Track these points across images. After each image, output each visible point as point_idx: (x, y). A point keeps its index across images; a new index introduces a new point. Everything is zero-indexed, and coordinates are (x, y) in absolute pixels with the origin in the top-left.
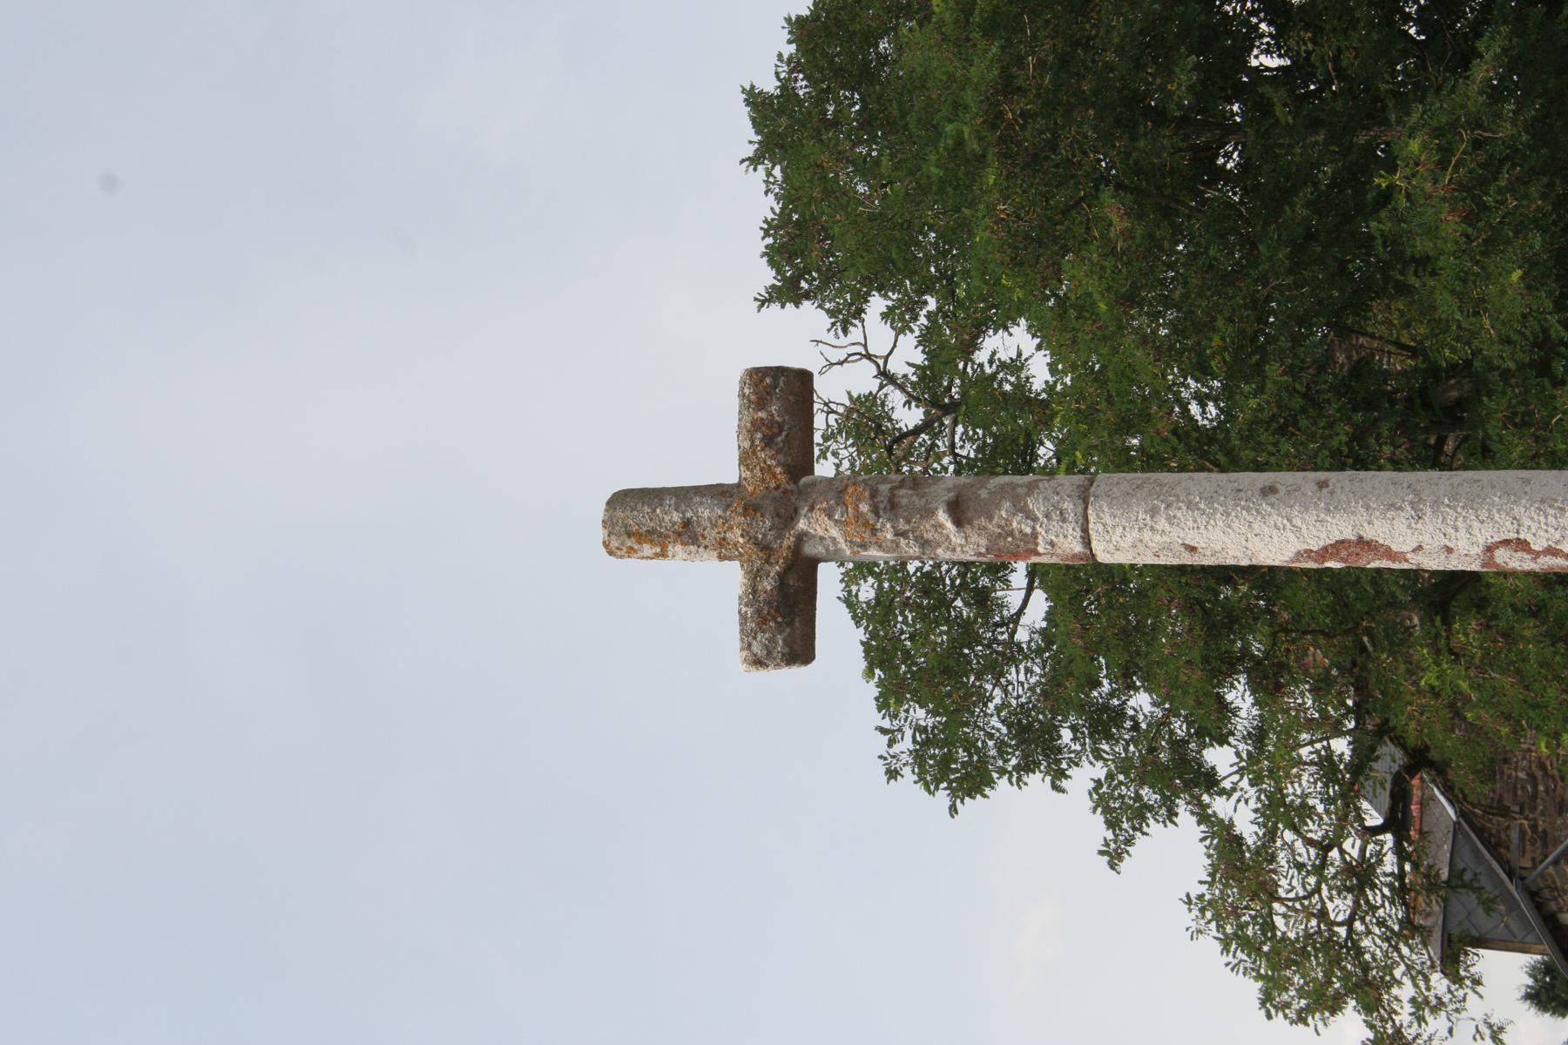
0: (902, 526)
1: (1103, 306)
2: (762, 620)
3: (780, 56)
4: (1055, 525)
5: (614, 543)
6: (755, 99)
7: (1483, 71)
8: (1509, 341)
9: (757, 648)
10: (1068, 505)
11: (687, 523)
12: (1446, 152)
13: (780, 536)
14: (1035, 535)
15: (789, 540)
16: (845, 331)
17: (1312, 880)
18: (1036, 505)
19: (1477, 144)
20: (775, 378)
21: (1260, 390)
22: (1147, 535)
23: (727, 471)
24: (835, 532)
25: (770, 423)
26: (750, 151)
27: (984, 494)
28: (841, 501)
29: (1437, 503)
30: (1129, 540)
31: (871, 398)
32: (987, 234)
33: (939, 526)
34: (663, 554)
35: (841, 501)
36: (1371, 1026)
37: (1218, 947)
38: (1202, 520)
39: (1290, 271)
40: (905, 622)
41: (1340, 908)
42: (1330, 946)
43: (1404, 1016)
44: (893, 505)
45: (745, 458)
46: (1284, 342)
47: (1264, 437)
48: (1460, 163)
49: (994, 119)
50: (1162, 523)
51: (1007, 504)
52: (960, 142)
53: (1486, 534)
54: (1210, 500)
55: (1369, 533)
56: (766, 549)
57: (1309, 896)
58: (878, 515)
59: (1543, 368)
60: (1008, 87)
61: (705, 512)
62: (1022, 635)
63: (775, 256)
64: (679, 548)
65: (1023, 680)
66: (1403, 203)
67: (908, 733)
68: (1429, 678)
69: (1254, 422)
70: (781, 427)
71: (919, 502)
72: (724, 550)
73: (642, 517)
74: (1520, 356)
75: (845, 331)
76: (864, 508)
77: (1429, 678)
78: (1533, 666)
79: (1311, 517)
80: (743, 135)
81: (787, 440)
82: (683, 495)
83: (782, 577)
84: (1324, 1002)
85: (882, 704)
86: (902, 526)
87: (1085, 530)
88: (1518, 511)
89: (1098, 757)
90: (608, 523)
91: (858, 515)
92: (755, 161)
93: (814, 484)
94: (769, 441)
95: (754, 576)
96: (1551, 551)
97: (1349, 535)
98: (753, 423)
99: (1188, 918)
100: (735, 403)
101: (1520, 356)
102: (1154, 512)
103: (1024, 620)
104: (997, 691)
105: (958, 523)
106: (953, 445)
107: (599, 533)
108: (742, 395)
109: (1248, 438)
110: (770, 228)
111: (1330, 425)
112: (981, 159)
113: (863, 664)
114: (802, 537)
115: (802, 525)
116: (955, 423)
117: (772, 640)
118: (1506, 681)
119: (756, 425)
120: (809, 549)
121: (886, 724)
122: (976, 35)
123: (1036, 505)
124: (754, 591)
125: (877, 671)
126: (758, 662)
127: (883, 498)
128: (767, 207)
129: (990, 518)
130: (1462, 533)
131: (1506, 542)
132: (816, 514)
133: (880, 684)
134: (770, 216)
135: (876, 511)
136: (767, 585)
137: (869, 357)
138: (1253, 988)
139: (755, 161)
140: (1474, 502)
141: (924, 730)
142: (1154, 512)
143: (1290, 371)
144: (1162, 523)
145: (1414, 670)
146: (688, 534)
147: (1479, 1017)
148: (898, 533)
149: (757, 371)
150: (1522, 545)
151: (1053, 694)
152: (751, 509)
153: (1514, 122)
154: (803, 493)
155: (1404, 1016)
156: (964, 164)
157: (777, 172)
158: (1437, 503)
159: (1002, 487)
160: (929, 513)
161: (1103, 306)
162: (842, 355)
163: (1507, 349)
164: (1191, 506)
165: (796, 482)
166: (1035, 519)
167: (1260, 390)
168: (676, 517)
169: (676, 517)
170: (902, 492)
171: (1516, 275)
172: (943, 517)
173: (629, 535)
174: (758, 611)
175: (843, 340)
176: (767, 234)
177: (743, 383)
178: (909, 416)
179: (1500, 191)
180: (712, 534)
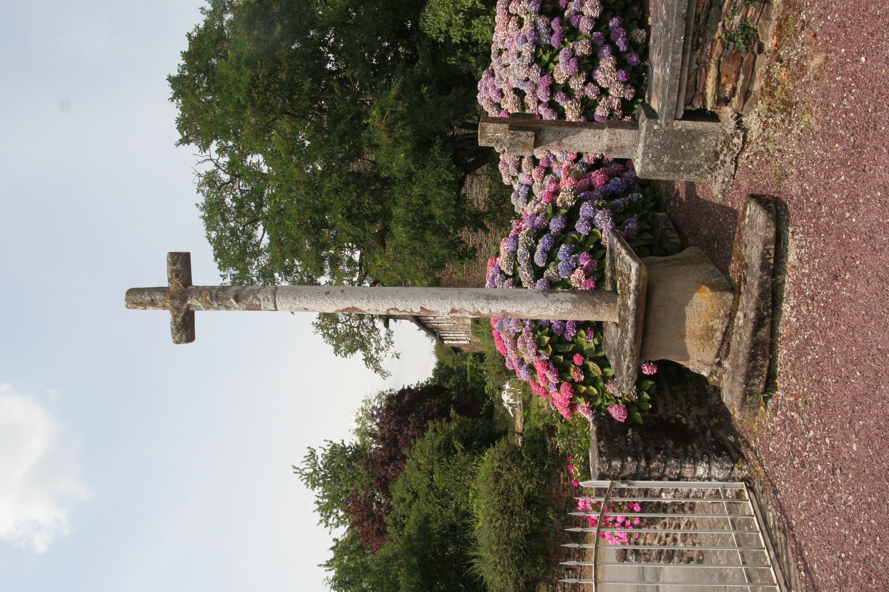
0: (220, 303)
1: (283, 155)
2: (178, 330)
3: (179, 65)
4: (266, 302)
5: (129, 306)
6: (171, 79)
7: (394, 92)
8: (400, 171)
9: (177, 338)
10: (269, 296)
11: (152, 300)
12: (383, 114)
13: (182, 305)
14: (260, 305)
15: (185, 307)
16: (205, 151)
17: (348, 317)
18: (260, 296)
19: (392, 112)
20: (178, 256)
21: (330, 181)
22: (293, 305)
23: (165, 283)
24: (199, 304)
25: (177, 271)
26: (171, 96)
27: (244, 293)
28: (200, 295)
29: (374, 298)
30: (288, 306)
31: (214, 172)
32: (247, 131)
33: (231, 303)
34: (145, 309)
35: (200, 295)
36: (365, 355)
37: (321, 336)
38: (309, 302)
39: (339, 145)
40: (226, 244)
41: (355, 324)
42: (354, 335)
43: (373, 352)
44: (217, 297)
45: (170, 280)
46: (337, 167)
47: (332, 195)
48: (387, 117)
49: (249, 92)
50: (297, 302)
51: (252, 296)
52: (239, 101)
53: (387, 307)
54: (311, 296)
55: (355, 306)
56: (178, 309)
57: (347, 321)
58: (212, 300)
59: (410, 178)
60: (253, 84)
61: (158, 297)
62: (262, 246)
63: (181, 128)
64: (150, 307)
65: (264, 260)
66: (371, 129)
67: (229, 276)
68: (379, 263)
69: (329, 190)
70: (181, 271)
71: (225, 296)
72: (164, 307)
73: (138, 298)
74: (403, 176)
75: (205, 151)
76: (208, 298)
77: (379, 263)
78: (407, 261)
79: (339, 301)
80: (169, 91)
81: (183, 276)
82: (151, 290)
83: (184, 317)
84: (352, 350)
85: (220, 267)
86: (220, 303)
87: (275, 304)
88: (395, 300)
89: (287, 280)
90: (127, 300)
91: (206, 300)
92: (172, 99)
93: (192, 289)
94: (177, 276)
95: (175, 317)
96: (404, 311)
97: (350, 306)
98: (172, 270)
99: (313, 328)
100: (166, 263)
101: (403, 176)
102: (295, 299)
103: (262, 242)
104: (256, 262)
105: (237, 302)
106: (239, 186)
107: (125, 303)
108: (168, 261)
109: (327, 195)
110: (178, 120)
111: (351, 192)
112: (245, 107)
113: (214, 257)
114: (189, 306)
115: (189, 302)
116: (240, 180)
117: (181, 336)
118: (400, 265)
119: (173, 271)
120: (191, 309)
121: (222, 273)
122: (243, 66)
123: (260, 296)
124: (175, 321)
125: (218, 259)
126: (178, 343)
127: (214, 295)
128: (178, 113)
129: (247, 300)
130: (381, 306)
131: (392, 309)
132: (193, 299)
133: (219, 263)
134: (178, 116)
135: (212, 299)
136: (179, 320)
137: (211, 160)
138: (332, 348)
139: (172, 99)
140: (384, 298)
141: (234, 275)
142: (295, 299)
143: (340, 176)
144: (297, 302)
145: (375, 260)
146: (153, 303)
147: (393, 352)
148: (219, 305)
149: (172, 253)
150: (397, 309)
151: (272, 261)
152: (172, 298)
153: (402, 106)
154: (189, 292)
155: (373, 352)
156: (240, 107)
157: (180, 101)
158: (374, 298)
159: (250, 290)
160: (228, 299)
161: (283, 155)
162: (204, 159)
163: (400, 174)
164: (305, 297)
165: (186, 288)
166: (260, 301)
167: (330, 181)
168: (149, 298)
169: (149, 298)
170: (220, 293)
171: (402, 155)
172: (232, 300)
173: (134, 303)
174: (177, 327)
175: (204, 154)
176: (177, 122)
177: (168, 257)
178: (226, 177)
179: (398, 127)
180: (160, 304)
